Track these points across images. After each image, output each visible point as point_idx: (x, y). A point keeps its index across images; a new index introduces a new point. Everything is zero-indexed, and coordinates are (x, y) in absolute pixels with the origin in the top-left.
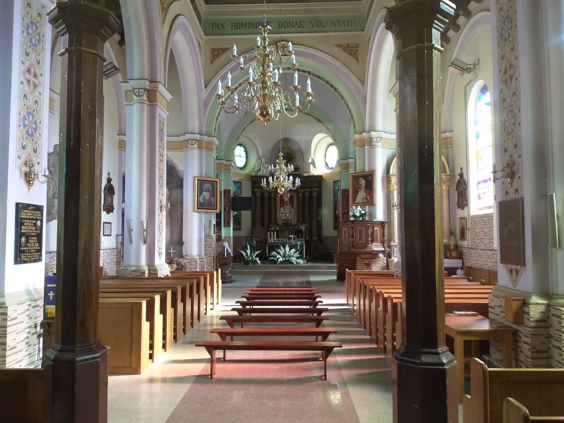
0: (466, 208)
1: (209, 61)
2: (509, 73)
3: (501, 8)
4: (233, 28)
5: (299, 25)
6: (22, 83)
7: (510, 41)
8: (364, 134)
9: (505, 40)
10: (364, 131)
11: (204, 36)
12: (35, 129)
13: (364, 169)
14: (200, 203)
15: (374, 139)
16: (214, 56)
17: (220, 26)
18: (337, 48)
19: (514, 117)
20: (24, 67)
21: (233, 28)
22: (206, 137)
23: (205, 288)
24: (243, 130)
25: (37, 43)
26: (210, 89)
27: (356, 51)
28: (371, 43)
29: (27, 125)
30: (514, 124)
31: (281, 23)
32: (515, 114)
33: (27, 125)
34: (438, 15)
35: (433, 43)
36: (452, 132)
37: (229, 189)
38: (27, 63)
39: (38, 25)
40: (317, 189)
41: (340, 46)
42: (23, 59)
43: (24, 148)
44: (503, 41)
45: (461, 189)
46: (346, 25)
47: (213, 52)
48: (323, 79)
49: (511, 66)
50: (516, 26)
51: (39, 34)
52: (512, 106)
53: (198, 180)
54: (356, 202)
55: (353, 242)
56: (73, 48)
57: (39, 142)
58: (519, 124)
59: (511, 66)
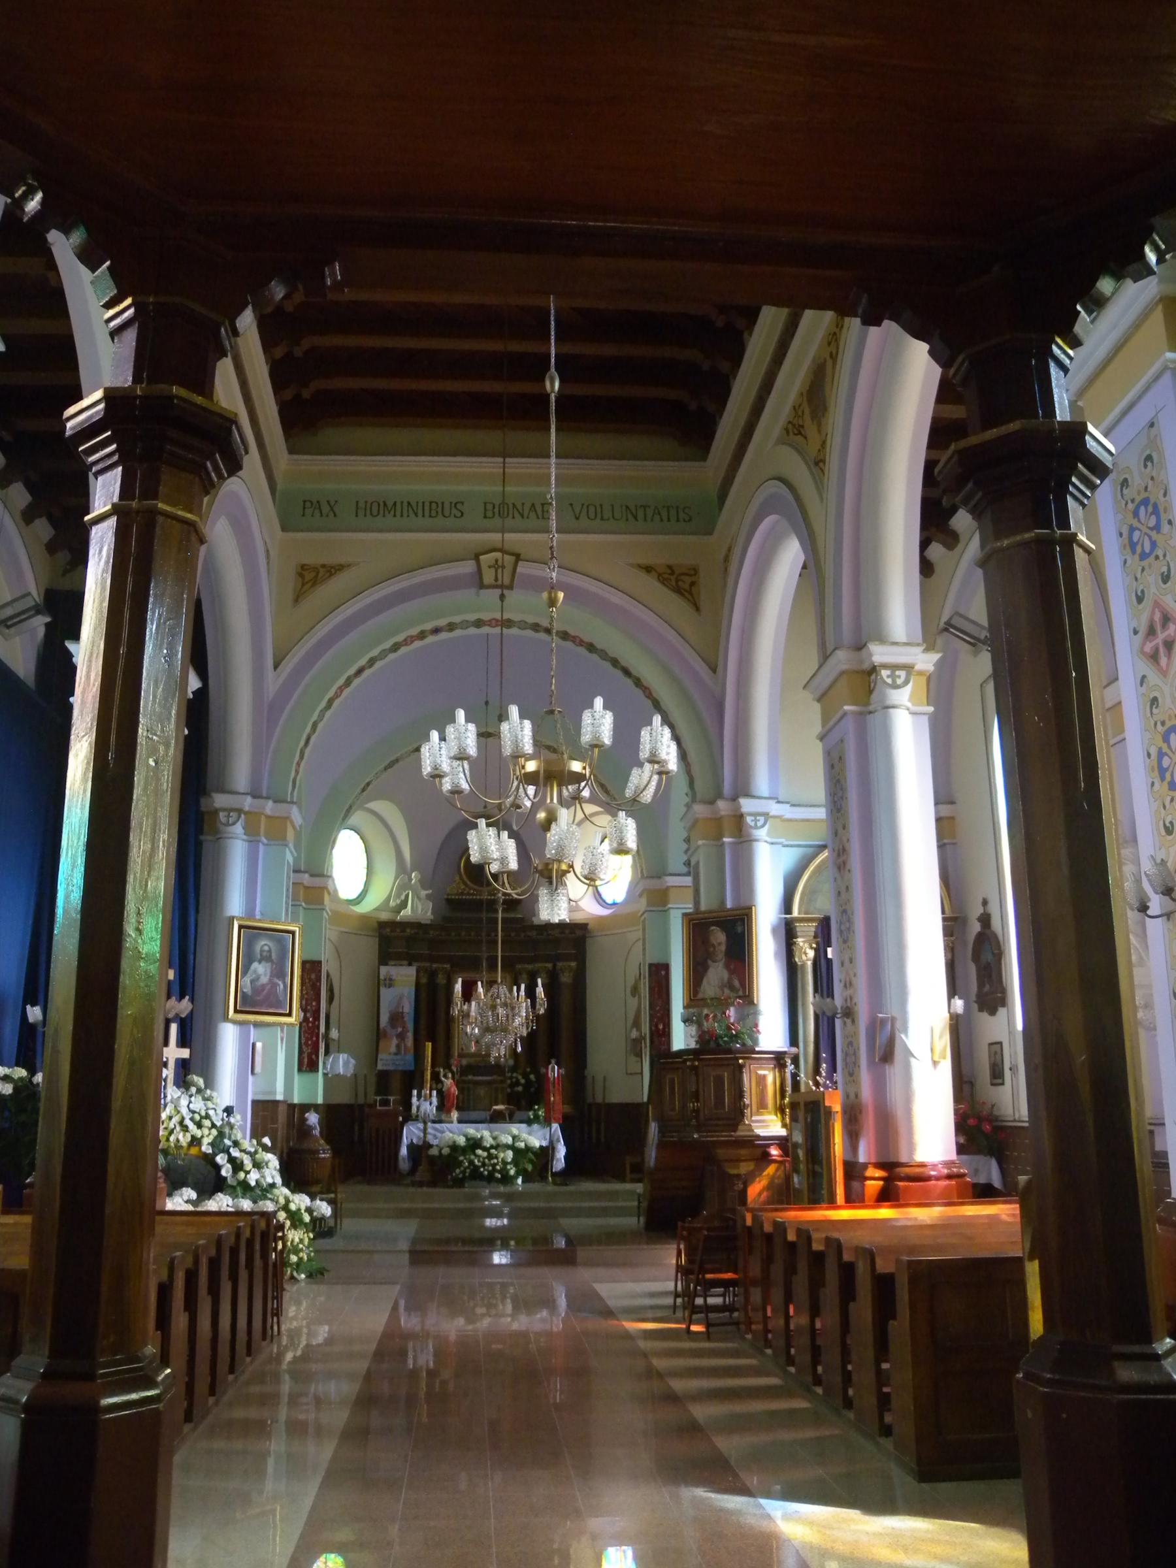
0: (1002, 1012)
2: (1161, 636)
3: (1126, 480)
4: (361, 513)
5: (540, 513)
7: (1157, 557)
8: (721, 804)
9: (1143, 556)
10: (719, 795)
13: (723, 902)
14: (244, 995)
15: (749, 819)
16: (303, 585)
17: (326, 509)
18: (643, 575)
22: (270, 804)
23: (234, 1278)
24: (363, 790)
27: (692, 584)
28: (732, 569)
31: (489, 507)
34: (1080, 465)
35: (1073, 529)
36: (952, 803)
37: (315, 958)
40: (573, 964)
41: (648, 569)
44: (1137, 557)
45: (987, 957)
47: (301, 575)
48: (603, 655)
53: (240, 927)
54: (700, 996)
55: (697, 1111)
56: (134, 504)
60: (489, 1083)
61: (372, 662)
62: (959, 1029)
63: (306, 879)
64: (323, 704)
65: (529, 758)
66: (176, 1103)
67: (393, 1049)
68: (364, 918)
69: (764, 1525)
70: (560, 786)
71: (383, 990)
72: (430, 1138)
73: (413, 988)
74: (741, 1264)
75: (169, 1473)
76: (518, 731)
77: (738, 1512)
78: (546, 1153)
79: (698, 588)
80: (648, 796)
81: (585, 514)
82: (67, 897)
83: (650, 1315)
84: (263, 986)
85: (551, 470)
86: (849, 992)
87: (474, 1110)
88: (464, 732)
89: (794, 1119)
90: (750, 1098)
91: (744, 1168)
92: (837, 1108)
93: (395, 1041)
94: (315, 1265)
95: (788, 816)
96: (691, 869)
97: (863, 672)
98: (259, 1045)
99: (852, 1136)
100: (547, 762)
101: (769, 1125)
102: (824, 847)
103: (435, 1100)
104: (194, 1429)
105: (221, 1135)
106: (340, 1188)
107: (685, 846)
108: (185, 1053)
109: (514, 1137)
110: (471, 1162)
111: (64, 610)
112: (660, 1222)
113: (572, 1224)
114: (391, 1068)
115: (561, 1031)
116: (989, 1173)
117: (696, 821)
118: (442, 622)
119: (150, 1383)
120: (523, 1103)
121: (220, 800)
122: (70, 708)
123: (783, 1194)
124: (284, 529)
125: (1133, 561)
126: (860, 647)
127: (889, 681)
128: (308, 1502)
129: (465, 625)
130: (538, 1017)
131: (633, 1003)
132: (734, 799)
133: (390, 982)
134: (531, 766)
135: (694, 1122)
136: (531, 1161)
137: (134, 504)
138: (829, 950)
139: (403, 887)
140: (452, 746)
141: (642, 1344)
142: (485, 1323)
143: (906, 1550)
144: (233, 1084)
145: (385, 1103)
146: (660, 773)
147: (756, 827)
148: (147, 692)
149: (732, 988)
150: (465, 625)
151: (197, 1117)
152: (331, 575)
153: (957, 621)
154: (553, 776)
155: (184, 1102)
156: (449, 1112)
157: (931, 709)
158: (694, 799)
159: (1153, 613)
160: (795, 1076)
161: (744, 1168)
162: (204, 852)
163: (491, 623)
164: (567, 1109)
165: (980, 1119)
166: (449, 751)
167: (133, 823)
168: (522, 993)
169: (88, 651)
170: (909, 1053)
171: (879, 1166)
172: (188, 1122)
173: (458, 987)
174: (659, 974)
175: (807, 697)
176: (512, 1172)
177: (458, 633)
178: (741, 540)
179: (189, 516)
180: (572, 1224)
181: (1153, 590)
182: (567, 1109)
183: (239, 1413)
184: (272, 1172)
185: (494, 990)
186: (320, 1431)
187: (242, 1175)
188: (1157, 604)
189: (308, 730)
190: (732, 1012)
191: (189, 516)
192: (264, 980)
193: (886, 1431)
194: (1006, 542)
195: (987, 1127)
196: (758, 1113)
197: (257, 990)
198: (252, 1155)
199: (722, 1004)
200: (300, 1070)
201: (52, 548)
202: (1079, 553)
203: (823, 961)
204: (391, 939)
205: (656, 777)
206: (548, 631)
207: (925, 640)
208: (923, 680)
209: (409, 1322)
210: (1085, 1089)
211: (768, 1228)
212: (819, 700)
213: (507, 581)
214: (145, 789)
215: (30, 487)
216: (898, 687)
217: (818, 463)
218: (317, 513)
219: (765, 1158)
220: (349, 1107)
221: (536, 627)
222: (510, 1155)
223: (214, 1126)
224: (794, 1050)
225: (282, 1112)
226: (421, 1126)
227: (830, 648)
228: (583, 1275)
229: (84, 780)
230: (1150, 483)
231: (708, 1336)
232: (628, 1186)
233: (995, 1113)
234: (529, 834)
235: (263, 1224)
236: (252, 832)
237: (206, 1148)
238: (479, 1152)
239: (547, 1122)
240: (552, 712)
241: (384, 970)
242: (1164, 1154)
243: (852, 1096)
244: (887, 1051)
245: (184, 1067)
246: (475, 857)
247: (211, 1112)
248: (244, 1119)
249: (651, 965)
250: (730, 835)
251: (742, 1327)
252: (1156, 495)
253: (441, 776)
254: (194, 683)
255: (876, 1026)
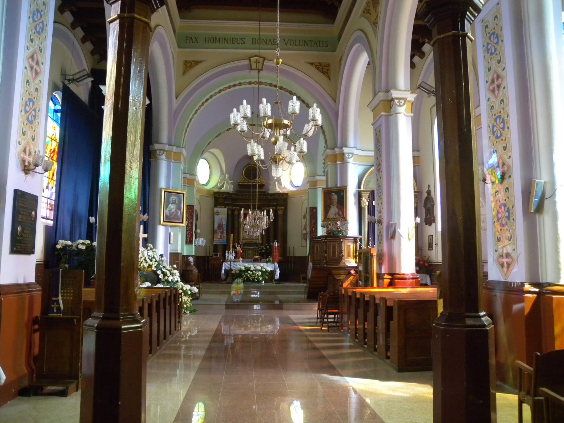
0: (433, 225)
1: (181, 72)
2: (496, 83)
4: (207, 42)
5: (272, 41)
6: (26, 68)
7: (496, 54)
8: (336, 149)
9: (497, 137)
10: (336, 147)
11: (177, 49)
12: (35, 117)
13: (337, 185)
14: (166, 216)
15: (346, 155)
17: (194, 40)
18: (309, 66)
19: (503, 122)
20: (29, 53)
21: (207, 42)
22: (175, 148)
24: (208, 144)
25: (40, 30)
26: (181, 99)
27: (328, 70)
29: (28, 112)
30: (503, 128)
31: (254, 40)
32: (503, 120)
33: (28, 112)
35: (466, 31)
36: (419, 151)
37: (191, 204)
38: (31, 50)
39: (42, 13)
40: (283, 207)
41: (312, 64)
42: (28, 44)
43: (24, 134)
44: (489, 54)
45: (429, 205)
46: (318, 45)
47: (185, 65)
49: (498, 77)
50: (502, 41)
51: (42, 23)
52: (500, 112)
53: (165, 192)
54: (328, 217)
55: (326, 257)
56: (126, 15)
57: (37, 130)
58: (508, 128)
59: (498, 77)
60: (253, 249)
61: (211, 97)
62: (418, 227)
63: (188, 176)
64: (194, 112)
65: (269, 118)
66: (143, 252)
67: (219, 237)
68: (209, 191)
69: (346, 384)
70: (280, 129)
71: (215, 216)
72: (232, 267)
73: (226, 216)
74: (340, 308)
75: (145, 368)
76: (266, 108)
77: (337, 381)
78: (273, 273)
79: (329, 71)
80: (311, 134)
81: (290, 43)
82: (105, 156)
83: (308, 324)
84: (173, 212)
85: (278, 26)
86: (380, 214)
87: (248, 258)
88: (246, 108)
89: (360, 259)
90: (345, 253)
91: (342, 277)
92: (375, 254)
93: (220, 234)
94: (193, 309)
95: (360, 154)
96: (326, 173)
97: (388, 100)
98: (172, 234)
99: (380, 264)
100: (275, 120)
101: (351, 262)
102: (373, 166)
103: (234, 254)
104: (153, 356)
105: (159, 264)
106: (201, 284)
107: (323, 165)
108: (146, 236)
109: (262, 267)
110: (247, 276)
111: (99, 76)
112: (312, 296)
113: (281, 297)
114: (218, 243)
115: (277, 230)
116: (427, 281)
117: (328, 155)
118: (237, 82)
119: (138, 322)
120: (265, 256)
121: (157, 146)
122: (102, 111)
123: (356, 284)
124: (179, 47)
125: (488, 56)
126: (388, 91)
127: (398, 104)
128: (192, 377)
129: (245, 83)
130: (270, 222)
131: (304, 222)
132: (341, 148)
133: (218, 214)
134: (270, 121)
135: (325, 261)
136: (267, 275)
137: (126, 15)
138: (374, 202)
139: (222, 180)
140: (242, 114)
141: (305, 333)
142: (252, 330)
143: (393, 390)
144: (163, 247)
145: (216, 255)
146: (315, 125)
147: (349, 158)
148: (132, 83)
149: (339, 215)
150: (245, 83)
151: (150, 258)
152: (196, 64)
153: (423, 85)
154: (277, 125)
155: (146, 252)
156: (239, 258)
157: (412, 114)
158: (327, 148)
159: (494, 75)
160: (360, 246)
161: (342, 277)
162: (151, 165)
163: (254, 83)
164: (280, 258)
165: (424, 262)
166: (239, 117)
167: (128, 130)
168: (265, 213)
169: (109, 89)
170: (400, 236)
171: (389, 274)
172: (147, 259)
173: (242, 212)
174: (313, 211)
175: (369, 110)
176: (261, 279)
177: (243, 86)
178: (347, 50)
179: (146, 20)
180: (281, 297)
181: (494, 66)
182: (280, 258)
183: (167, 352)
184: (177, 277)
185: (255, 213)
186: (195, 357)
187: (166, 278)
188: (495, 72)
189: (188, 121)
190: (339, 223)
191: (146, 20)
192: (173, 210)
193: (388, 358)
194: (442, 36)
195: (427, 264)
196: (347, 258)
197: (171, 214)
198: (170, 271)
199: (335, 220)
200: (186, 243)
201: (93, 53)
202: (468, 40)
203: (371, 207)
204: (219, 198)
205: (314, 127)
206: (276, 86)
207: (411, 89)
208: (410, 104)
209: (225, 329)
210: (461, 229)
211: (350, 294)
212: (372, 111)
213: (260, 68)
214: (132, 118)
215: (83, 29)
216: (401, 106)
217: (375, 24)
218: (191, 41)
219: (349, 274)
220: (204, 257)
221: (271, 85)
222: (260, 273)
223: (156, 261)
224: (360, 236)
225: (180, 258)
226: (229, 263)
227: (377, 91)
228: (285, 313)
229: (110, 114)
230: (502, 110)
231: (328, 331)
232: (301, 284)
233: (430, 260)
234: (269, 146)
235: (174, 292)
236: (168, 158)
237: (154, 268)
238: (249, 272)
239: (273, 262)
240: (277, 103)
241: (216, 209)
242: (487, 273)
243: (380, 250)
244: (393, 235)
245: (145, 240)
246: (249, 153)
247: (155, 256)
248: (167, 258)
249: (310, 208)
250: (338, 159)
251: (340, 328)
252: (498, 31)
253: (237, 125)
254: (148, 102)
255: (389, 226)
